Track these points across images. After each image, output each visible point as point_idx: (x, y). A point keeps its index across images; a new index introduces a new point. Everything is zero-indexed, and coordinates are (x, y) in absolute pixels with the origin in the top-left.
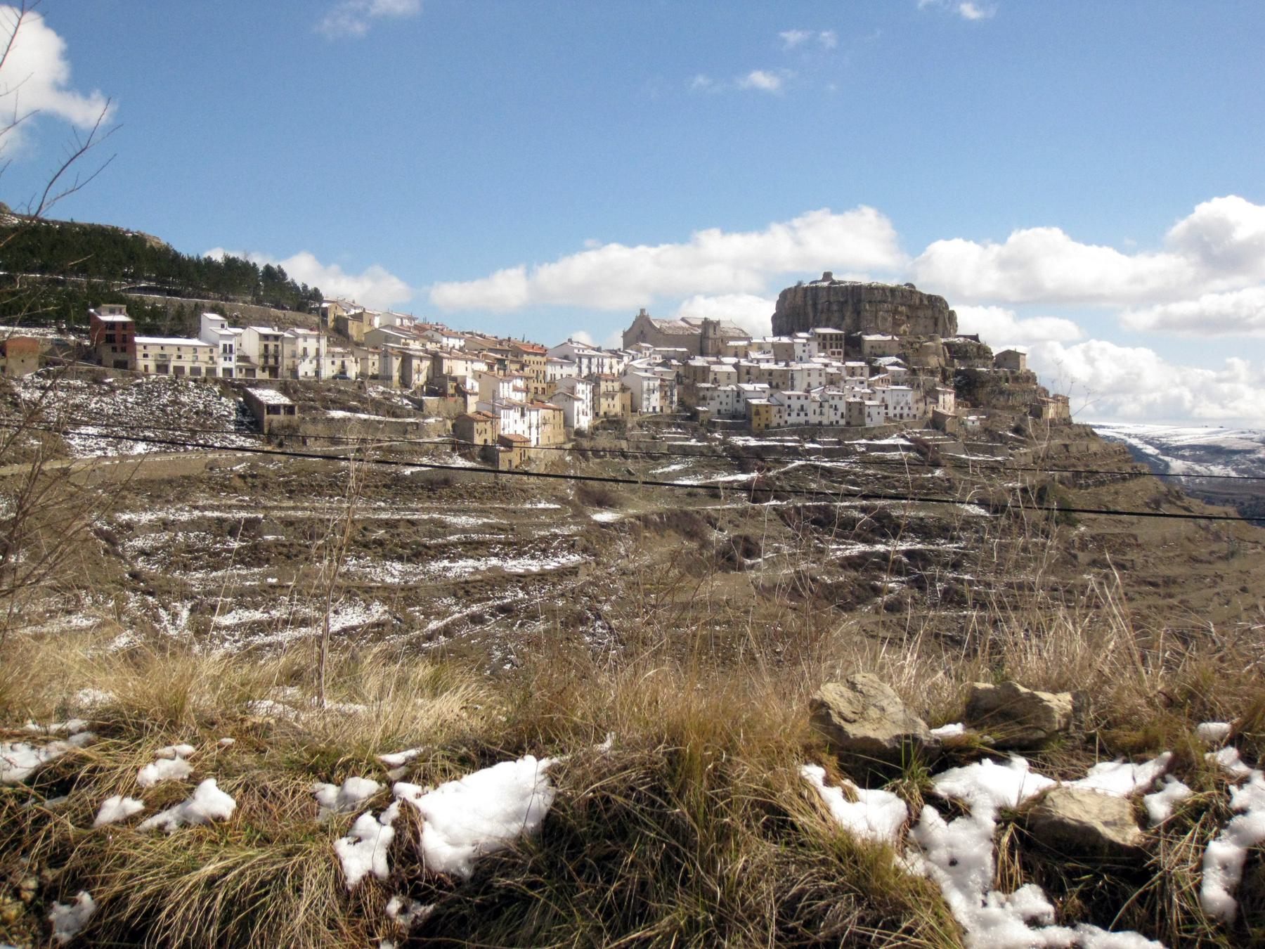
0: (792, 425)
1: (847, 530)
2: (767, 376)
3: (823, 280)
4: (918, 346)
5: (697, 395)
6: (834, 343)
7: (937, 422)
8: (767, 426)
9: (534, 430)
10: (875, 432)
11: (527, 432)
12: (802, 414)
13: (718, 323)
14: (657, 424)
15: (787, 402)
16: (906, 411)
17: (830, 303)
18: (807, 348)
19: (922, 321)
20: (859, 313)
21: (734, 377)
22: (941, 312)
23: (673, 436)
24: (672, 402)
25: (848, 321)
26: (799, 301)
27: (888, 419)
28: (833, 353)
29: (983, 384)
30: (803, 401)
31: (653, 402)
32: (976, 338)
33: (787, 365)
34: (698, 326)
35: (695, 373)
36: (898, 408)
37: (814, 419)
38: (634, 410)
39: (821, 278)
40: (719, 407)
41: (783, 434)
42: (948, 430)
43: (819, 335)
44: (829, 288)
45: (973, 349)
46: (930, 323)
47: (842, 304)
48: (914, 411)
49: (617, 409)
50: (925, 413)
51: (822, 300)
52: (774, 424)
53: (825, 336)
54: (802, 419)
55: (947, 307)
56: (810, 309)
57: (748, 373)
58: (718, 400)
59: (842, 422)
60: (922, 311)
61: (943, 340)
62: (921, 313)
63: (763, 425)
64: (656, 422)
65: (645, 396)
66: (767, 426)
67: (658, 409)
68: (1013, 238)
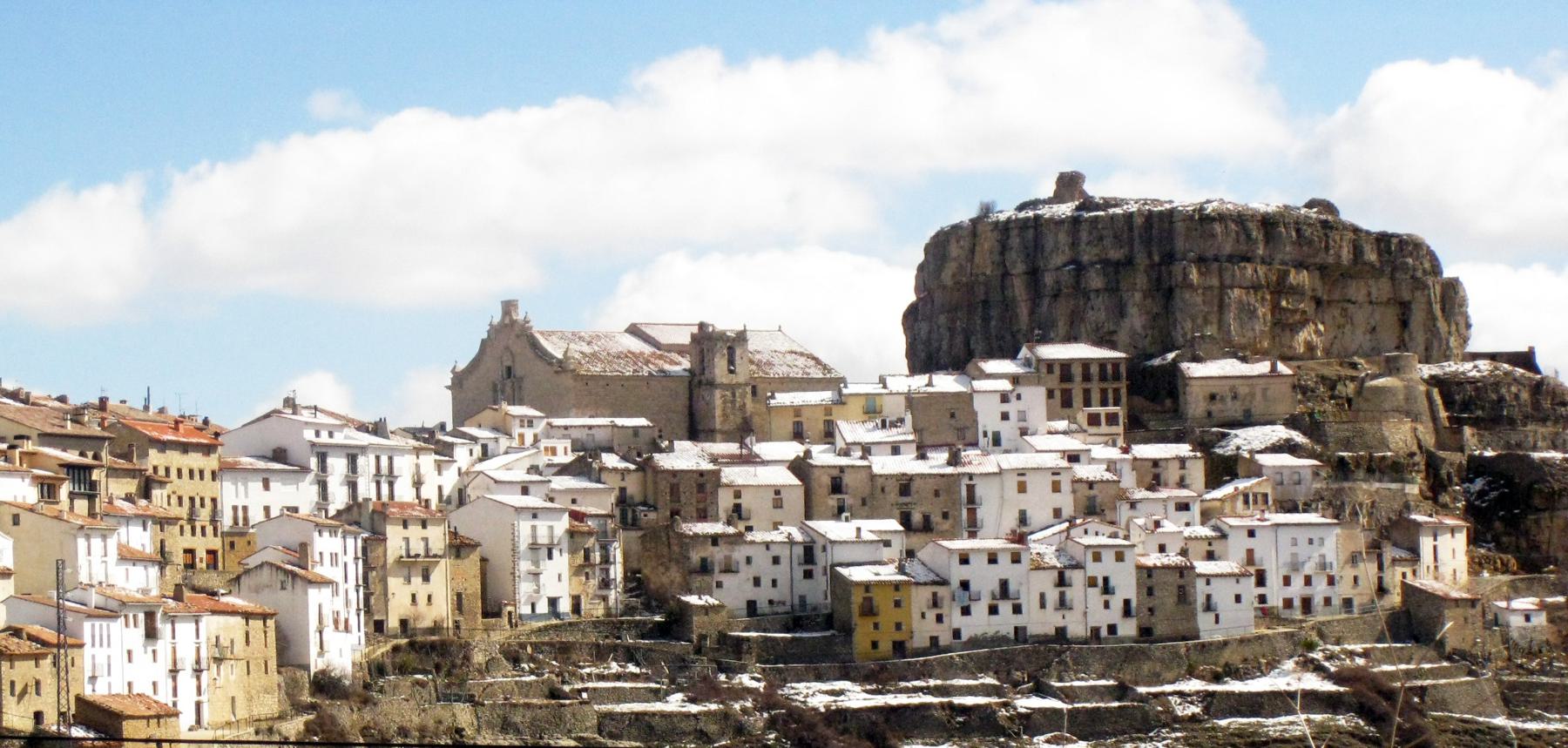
0: (974, 642)
2: (893, 495)
3: (1058, 198)
6: (1095, 388)
7: (1414, 621)
8: (899, 648)
9: (186, 680)
12: (1005, 607)
13: (741, 337)
14: (563, 650)
15: (957, 573)
17: (1080, 268)
18: (1012, 408)
19: (1361, 315)
21: (795, 500)
22: (1419, 285)
24: (606, 584)
25: (1136, 320)
26: (985, 262)
27: (1266, 613)
28: (1094, 420)
29: (1552, 500)
30: (1005, 568)
32: (1526, 360)
33: (954, 460)
34: (681, 350)
35: (674, 490)
36: (1297, 582)
37: (1040, 622)
38: (491, 610)
39: (1047, 189)
40: (750, 592)
41: (949, 669)
43: (1050, 365)
46: (1390, 316)
47: (1117, 270)
48: (1344, 589)
50: (1382, 590)
51: (1057, 258)
52: (920, 641)
53: (1066, 366)
54: (1005, 622)
55: (1436, 269)
56: (1018, 288)
57: (837, 487)
58: (746, 573)
59: (1128, 629)
61: (1427, 370)
63: (886, 646)
64: (559, 644)
65: (525, 566)
66: (899, 648)
67: (565, 606)
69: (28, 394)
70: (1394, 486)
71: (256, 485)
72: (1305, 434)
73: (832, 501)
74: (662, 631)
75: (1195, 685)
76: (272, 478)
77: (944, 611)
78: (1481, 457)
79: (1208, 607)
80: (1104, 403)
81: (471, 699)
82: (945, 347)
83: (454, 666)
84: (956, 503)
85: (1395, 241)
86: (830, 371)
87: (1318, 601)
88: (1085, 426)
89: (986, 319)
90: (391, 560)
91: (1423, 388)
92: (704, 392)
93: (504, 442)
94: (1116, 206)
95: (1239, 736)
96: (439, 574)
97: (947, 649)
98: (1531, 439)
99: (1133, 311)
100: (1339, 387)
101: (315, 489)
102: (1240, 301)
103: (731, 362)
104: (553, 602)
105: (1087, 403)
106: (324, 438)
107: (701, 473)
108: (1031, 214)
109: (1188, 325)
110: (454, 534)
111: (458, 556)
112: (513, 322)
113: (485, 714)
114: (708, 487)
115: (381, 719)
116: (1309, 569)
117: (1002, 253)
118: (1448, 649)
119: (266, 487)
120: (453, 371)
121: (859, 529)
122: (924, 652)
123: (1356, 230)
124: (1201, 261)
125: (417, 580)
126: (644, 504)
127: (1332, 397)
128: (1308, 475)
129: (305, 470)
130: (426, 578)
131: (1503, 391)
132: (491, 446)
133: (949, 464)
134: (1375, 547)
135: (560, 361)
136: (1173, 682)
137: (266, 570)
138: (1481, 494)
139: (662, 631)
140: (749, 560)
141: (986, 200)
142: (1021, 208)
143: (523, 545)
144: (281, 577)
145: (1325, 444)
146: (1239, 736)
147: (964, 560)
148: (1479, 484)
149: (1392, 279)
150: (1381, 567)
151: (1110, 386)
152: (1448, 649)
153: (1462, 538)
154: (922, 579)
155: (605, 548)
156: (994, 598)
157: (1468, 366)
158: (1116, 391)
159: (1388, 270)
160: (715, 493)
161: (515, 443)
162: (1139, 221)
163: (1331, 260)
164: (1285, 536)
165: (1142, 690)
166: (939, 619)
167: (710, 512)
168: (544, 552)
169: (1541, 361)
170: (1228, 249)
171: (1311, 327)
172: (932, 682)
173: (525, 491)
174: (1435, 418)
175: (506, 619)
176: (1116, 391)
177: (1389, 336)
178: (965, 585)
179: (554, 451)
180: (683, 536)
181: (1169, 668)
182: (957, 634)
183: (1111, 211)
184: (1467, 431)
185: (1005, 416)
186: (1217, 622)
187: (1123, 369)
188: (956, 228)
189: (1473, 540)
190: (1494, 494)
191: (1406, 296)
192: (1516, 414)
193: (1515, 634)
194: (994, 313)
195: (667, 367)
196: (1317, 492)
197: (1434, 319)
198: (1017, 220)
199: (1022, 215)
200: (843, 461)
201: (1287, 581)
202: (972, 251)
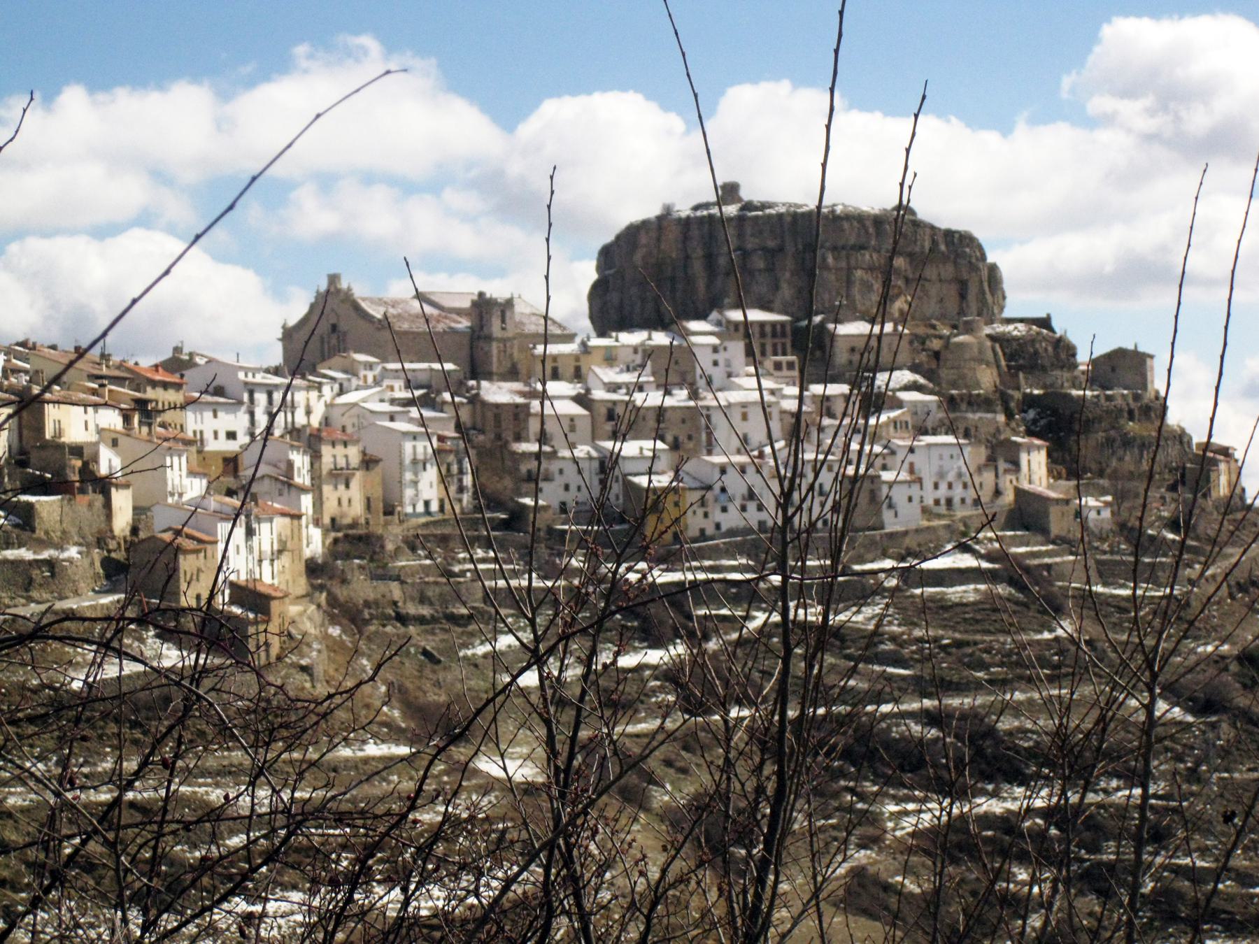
0: (732, 533)
1: (909, 766)
3: (720, 203)
4: (936, 344)
5: (514, 471)
6: (769, 342)
7: (1028, 514)
9: (266, 564)
10: (909, 542)
11: (257, 570)
13: (509, 303)
14: (444, 540)
16: (958, 492)
17: (746, 254)
18: (721, 357)
19: (934, 290)
20: (812, 275)
21: (584, 427)
22: (973, 268)
23: (477, 564)
25: (786, 292)
27: (925, 511)
28: (778, 366)
29: (1088, 426)
31: (425, 490)
32: (1045, 323)
34: (459, 312)
35: (497, 418)
36: (943, 486)
38: (389, 511)
40: (563, 496)
41: (715, 553)
42: (1055, 529)
44: (740, 220)
45: (1039, 350)
46: (952, 291)
47: (773, 254)
49: (357, 510)
50: (997, 493)
52: (693, 532)
56: (698, 267)
57: (611, 416)
58: (559, 481)
60: (930, 266)
61: (987, 330)
62: (930, 272)
64: (433, 537)
65: (408, 476)
67: (434, 507)
68: (558, 113)
69: (34, 344)
70: (989, 416)
71: (208, 415)
72: (924, 377)
73: (609, 427)
74: (505, 525)
75: (888, 564)
76: (218, 408)
77: (709, 509)
78: (1031, 393)
79: (890, 506)
80: (784, 354)
81: (398, 578)
82: (637, 309)
83: (375, 553)
84: (698, 429)
85: (957, 236)
86: (564, 328)
87: (957, 500)
88: (772, 371)
89: (673, 290)
90: (324, 472)
91: (989, 343)
92: (481, 344)
93: (355, 382)
94: (770, 207)
95: (932, 601)
96: (355, 483)
97: (712, 538)
98: (1059, 382)
99: (784, 286)
100: (928, 342)
101: (247, 417)
102: (862, 280)
103: (503, 321)
104: (427, 503)
105: (775, 354)
106: (250, 379)
107: (517, 406)
108: (705, 213)
109: (826, 296)
110: (364, 453)
111: (367, 469)
112: (338, 291)
113: (409, 589)
114: (522, 416)
115: (352, 594)
116: (951, 477)
117: (684, 242)
118: (1052, 536)
119: (215, 416)
120: (284, 327)
121: (641, 449)
122: (695, 540)
123: (933, 228)
124: (834, 249)
125: (342, 487)
126: (474, 428)
127: (923, 350)
128: (934, 408)
129: (240, 403)
130: (347, 486)
131: (1037, 346)
132: (345, 384)
133: (690, 398)
134: (992, 460)
135: (380, 321)
136: (872, 561)
137: (267, 481)
138: (1035, 421)
139: (505, 525)
140: (561, 471)
141: (668, 201)
142: (696, 208)
143: (407, 461)
144: (279, 486)
145: (939, 384)
146: (932, 601)
147: (723, 471)
148: (1031, 414)
149: (955, 263)
150: (997, 476)
151: (778, 341)
152: (1052, 536)
153: (1043, 453)
154: (694, 485)
155: (460, 462)
156: (744, 498)
157: (1010, 327)
158: (784, 345)
159: (952, 257)
160: (526, 421)
161: (361, 383)
162: (789, 219)
163: (917, 249)
164: (935, 453)
165: (857, 567)
166: (706, 515)
167: (523, 435)
168: (421, 466)
169: (1055, 324)
170: (852, 241)
171: (902, 298)
172: (707, 563)
173: (392, 419)
174: (998, 367)
175: (396, 517)
176: (784, 345)
177: (952, 305)
178: (723, 490)
179: (392, 388)
180: (514, 453)
181: (869, 551)
182: (718, 526)
183: (768, 211)
184: (1021, 375)
185: (716, 363)
186: (896, 515)
187: (788, 329)
188: (645, 223)
189: (1049, 455)
190: (1043, 422)
191: (965, 276)
192: (1047, 363)
193: (1091, 524)
194: (680, 286)
195: (453, 325)
196: (941, 420)
197: (983, 293)
198: (696, 218)
199: (699, 213)
200: (614, 397)
201: (936, 486)
202: (659, 240)
